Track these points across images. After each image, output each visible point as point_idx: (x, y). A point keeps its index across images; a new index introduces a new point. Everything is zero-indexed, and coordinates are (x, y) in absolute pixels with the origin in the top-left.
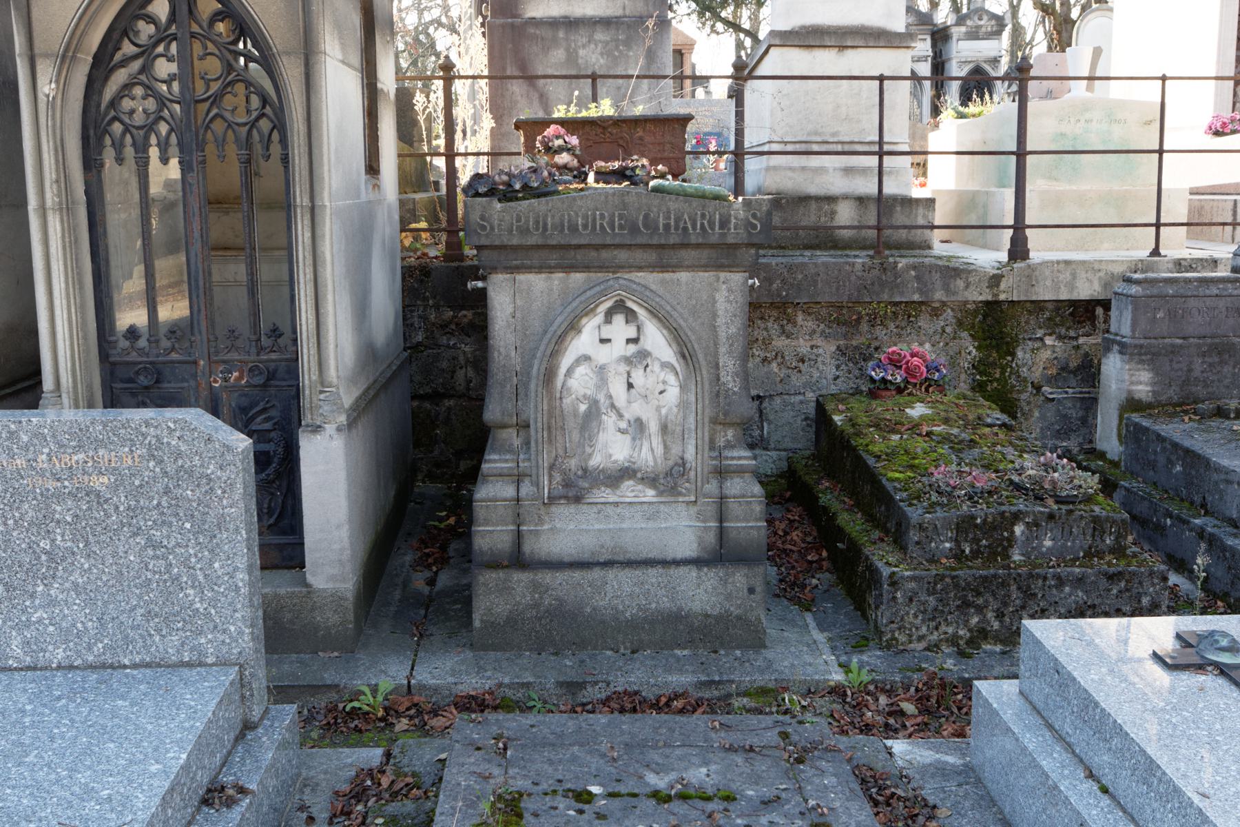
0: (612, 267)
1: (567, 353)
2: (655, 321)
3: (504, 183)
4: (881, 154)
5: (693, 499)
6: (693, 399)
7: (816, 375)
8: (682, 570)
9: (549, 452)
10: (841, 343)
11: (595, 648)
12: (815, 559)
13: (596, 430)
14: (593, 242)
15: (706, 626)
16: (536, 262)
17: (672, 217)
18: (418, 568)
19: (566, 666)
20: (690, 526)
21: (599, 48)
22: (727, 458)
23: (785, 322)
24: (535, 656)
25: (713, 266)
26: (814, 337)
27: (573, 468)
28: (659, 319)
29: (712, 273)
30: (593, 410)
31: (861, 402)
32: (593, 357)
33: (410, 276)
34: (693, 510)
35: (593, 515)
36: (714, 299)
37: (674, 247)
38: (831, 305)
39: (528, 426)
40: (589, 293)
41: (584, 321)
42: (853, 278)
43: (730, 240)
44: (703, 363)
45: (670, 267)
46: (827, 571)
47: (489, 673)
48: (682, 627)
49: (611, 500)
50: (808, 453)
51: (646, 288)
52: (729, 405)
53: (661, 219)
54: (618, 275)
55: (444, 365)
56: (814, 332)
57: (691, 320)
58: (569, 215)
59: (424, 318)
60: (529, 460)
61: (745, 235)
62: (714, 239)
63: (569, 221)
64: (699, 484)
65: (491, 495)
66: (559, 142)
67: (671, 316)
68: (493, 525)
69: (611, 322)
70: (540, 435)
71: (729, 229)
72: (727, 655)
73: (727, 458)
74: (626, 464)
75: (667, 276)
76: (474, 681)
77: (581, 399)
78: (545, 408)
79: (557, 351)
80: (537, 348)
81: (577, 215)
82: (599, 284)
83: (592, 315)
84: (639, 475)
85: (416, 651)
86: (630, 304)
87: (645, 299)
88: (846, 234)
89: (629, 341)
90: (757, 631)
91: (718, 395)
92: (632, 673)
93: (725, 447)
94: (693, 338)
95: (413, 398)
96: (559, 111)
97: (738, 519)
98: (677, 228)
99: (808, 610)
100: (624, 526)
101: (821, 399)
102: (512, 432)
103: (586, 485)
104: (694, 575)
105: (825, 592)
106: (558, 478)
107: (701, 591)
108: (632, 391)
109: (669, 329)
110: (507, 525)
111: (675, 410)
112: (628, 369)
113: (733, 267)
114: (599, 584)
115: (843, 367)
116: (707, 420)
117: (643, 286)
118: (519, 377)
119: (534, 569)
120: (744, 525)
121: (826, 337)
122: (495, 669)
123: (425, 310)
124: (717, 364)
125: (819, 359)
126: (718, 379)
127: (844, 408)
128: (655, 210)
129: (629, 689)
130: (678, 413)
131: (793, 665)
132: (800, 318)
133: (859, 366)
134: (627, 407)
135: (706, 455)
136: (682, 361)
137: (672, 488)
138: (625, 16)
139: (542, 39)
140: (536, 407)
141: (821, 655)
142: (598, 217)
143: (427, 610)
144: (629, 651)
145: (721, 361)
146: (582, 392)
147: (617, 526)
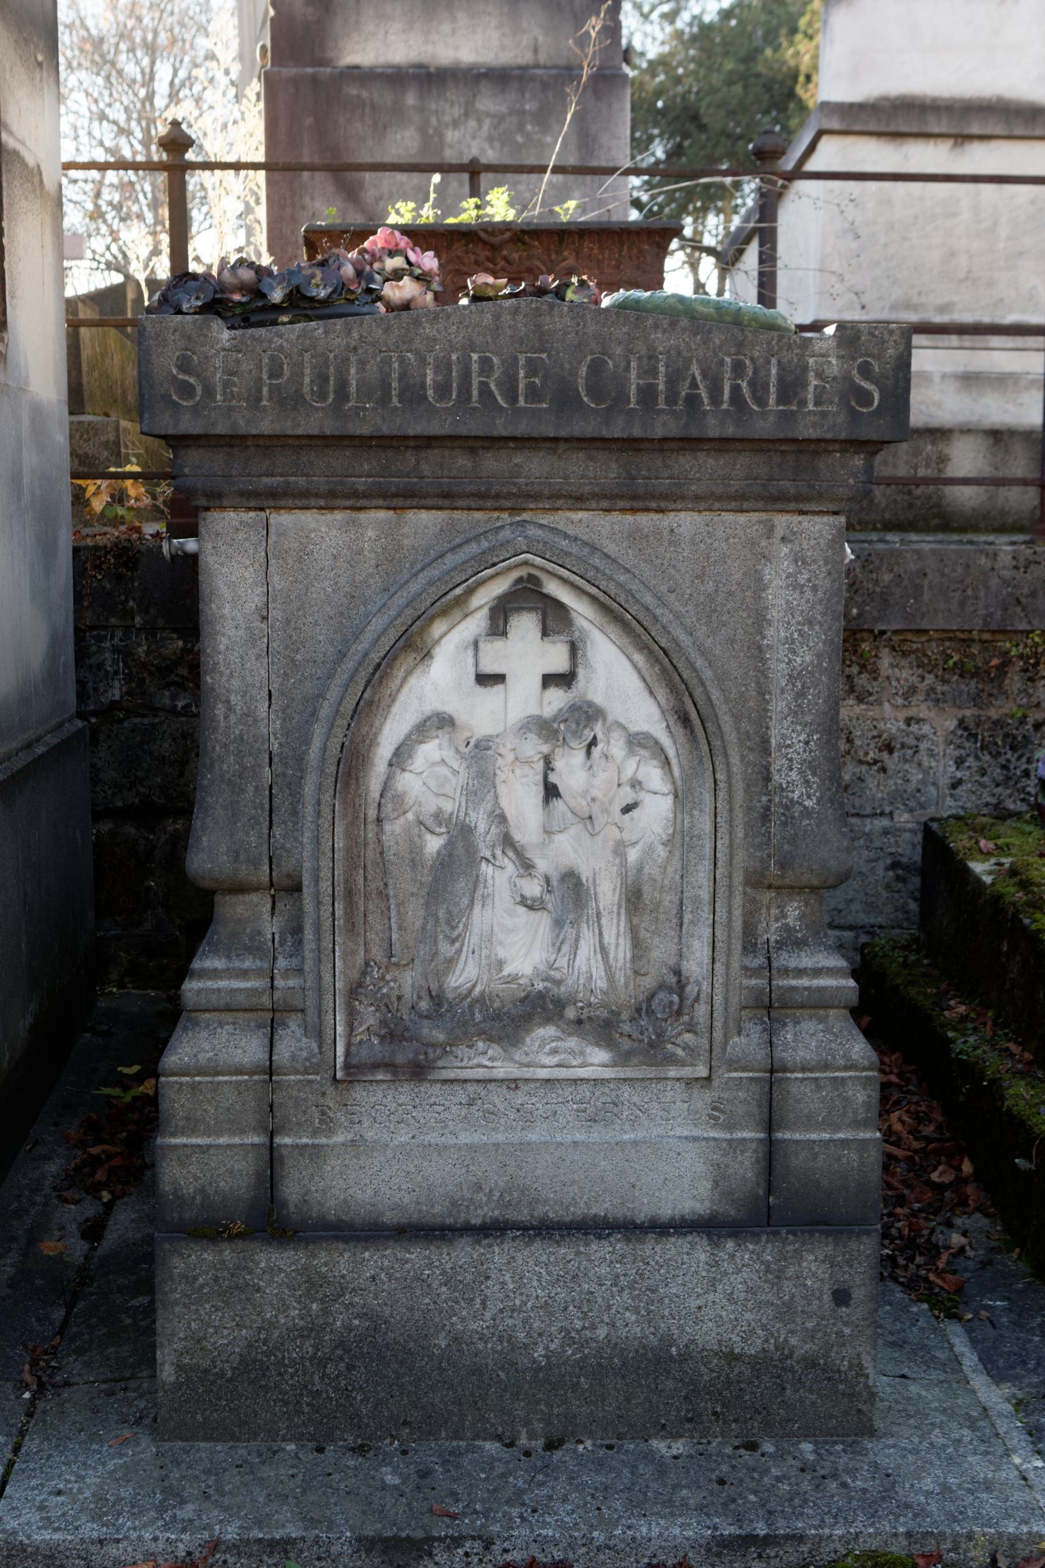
0: (510, 495)
1: (395, 709)
2: (614, 631)
3: (242, 288)
4: (273, 1010)
5: (702, 1071)
6: (707, 827)
7: (916, 776)
8: (675, 1246)
9: (349, 954)
10: (968, 713)
11: (457, 1436)
12: (947, 1179)
13: (465, 901)
14: (463, 431)
15: (728, 1383)
16: (320, 482)
17: (662, 369)
18: (66, 1194)
19: (384, 1487)
20: (695, 1139)
21: (485, 128)
22: (785, 972)
23: (855, 669)
24: (308, 1456)
25: (759, 498)
26: (914, 700)
27: (407, 992)
28: (625, 626)
29: (755, 516)
30: (460, 850)
31: (1023, 833)
32: (460, 717)
33: (95, 567)
34: (703, 1099)
35: (455, 1109)
36: (760, 579)
37: (664, 445)
38: (948, 635)
39: (298, 888)
40: (450, 561)
41: (438, 628)
42: (994, 582)
43: (805, 430)
44: (731, 736)
45: (653, 497)
46: (977, 1209)
47: (187, 1512)
48: (670, 1384)
49: (500, 1073)
50: (903, 936)
51: (593, 548)
52: (793, 840)
53: (633, 375)
54: (526, 516)
55: (166, 747)
56: (913, 690)
57: (701, 631)
58: (402, 360)
59: (125, 653)
60: (300, 971)
61: (841, 419)
62: (764, 427)
63: (402, 376)
64: (718, 1035)
65: (203, 1058)
66: (398, 262)
67: (656, 619)
68: (208, 1133)
69: (504, 634)
70: (325, 913)
71: (803, 403)
72: (780, 1455)
73: (785, 972)
74: (540, 986)
75: (645, 520)
76: (148, 1536)
77: (430, 822)
78: (340, 844)
79: (370, 703)
80: (321, 696)
81: (423, 361)
82: (476, 538)
83: (457, 614)
84: (571, 1013)
85: (22, 1433)
86: (553, 588)
87: (591, 574)
88: (965, 497)
89: (549, 680)
90: (852, 1396)
91: (765, 817)
92: (549, 1511)
93: (781, 945)
94: (708, 674)
95: (97, 816)
96: (398, 212)
97: (810, 1122)
98: (672, 398)
99: (957, 1317)
100: (533, 1137)
101: (935, 826)
102: (262, 902)
103: (440, 1036)
104: (703, 1257)
105: (985, 1264)
106: (370, 1017)
107: (719, 1296)
108: (558, 804)
109: (651, 652)
110: (243, 1132)
111: (661, 852)
112: (545, 749)
113: (808, 499)
114: (469, 1277)
115: (970, 761)
116: (738, 878)
117: (585, 544)
118: (278, 768)
119: (308, 1241)
120: (826, 1136)
121: (937, 700)
122: (207, 1496)
123: (126, 637)
124: (765, 741)
125: (924, 746)
126: (768, 779)
127: (991, 845)
128: (619, 351)
129: (540, 1557)
130: (668, 860)
131: (945, 1488)
132: (885, 661)
133: (1002, 760)
134: (543, 844)
135: (736, 965)
136: (679, 730)
137: (651, 1045)
138: (537, 66)
139: (374, 108)
140: (317, 842)
141: (1007, 1453)
142: (475, 367)
143: (70, 1307)
144: (540, 1443)
145: (773, 732)
146: (431, 805)
147: (516, 1137)
